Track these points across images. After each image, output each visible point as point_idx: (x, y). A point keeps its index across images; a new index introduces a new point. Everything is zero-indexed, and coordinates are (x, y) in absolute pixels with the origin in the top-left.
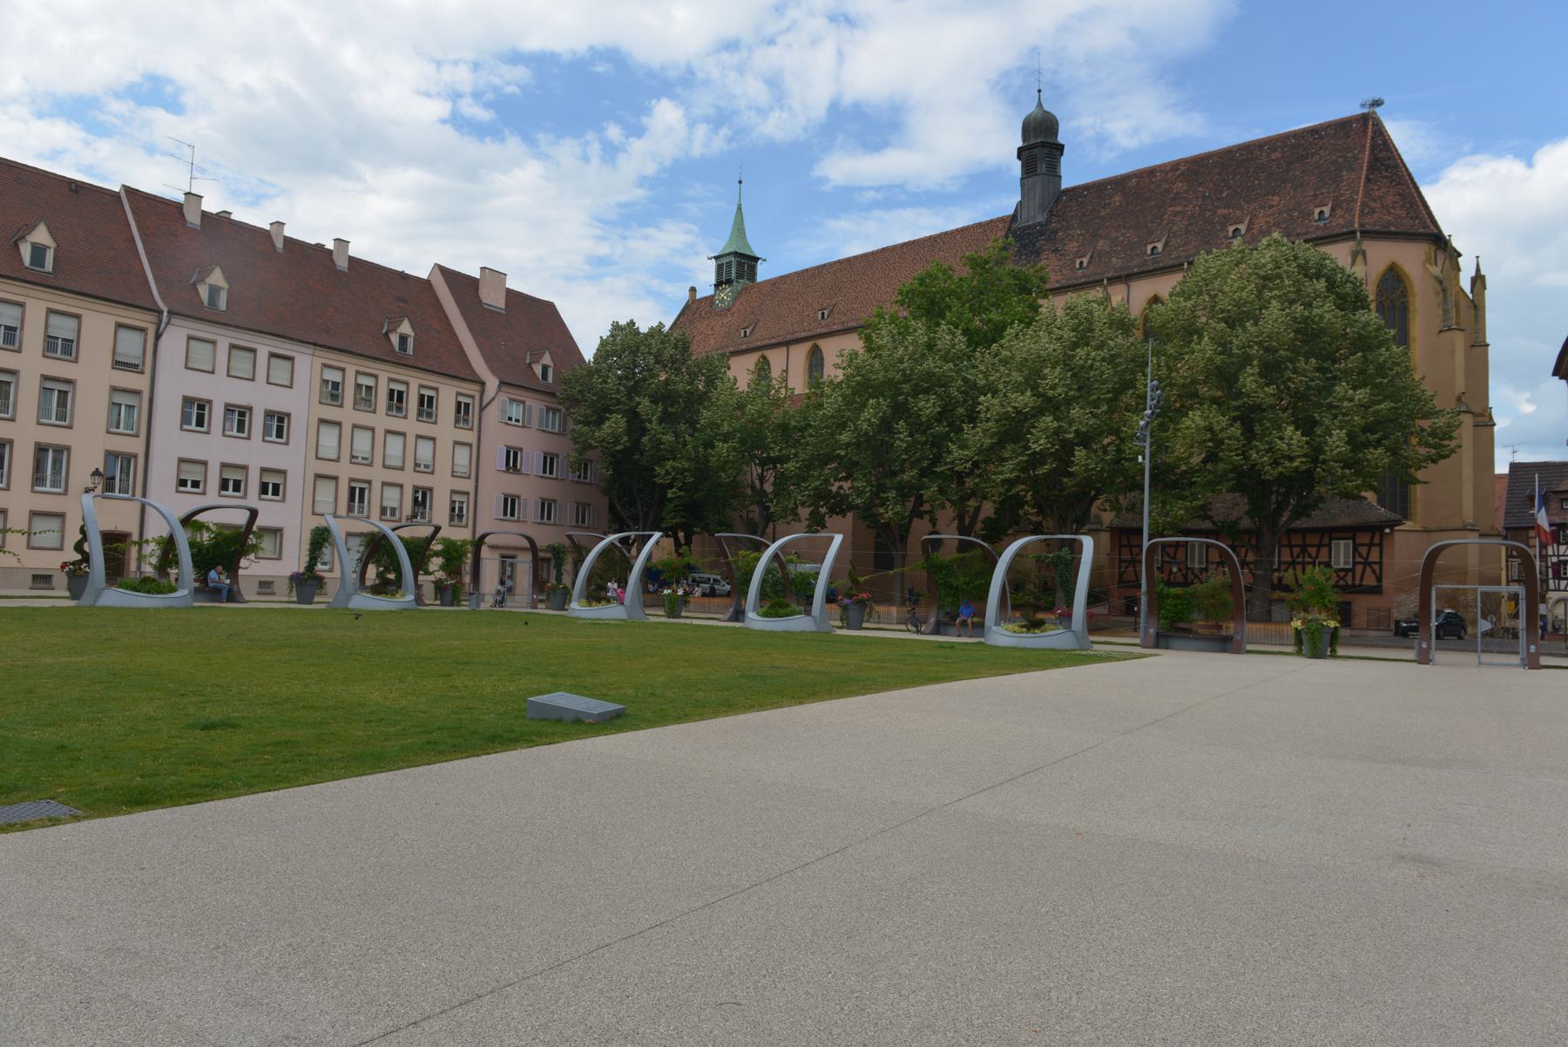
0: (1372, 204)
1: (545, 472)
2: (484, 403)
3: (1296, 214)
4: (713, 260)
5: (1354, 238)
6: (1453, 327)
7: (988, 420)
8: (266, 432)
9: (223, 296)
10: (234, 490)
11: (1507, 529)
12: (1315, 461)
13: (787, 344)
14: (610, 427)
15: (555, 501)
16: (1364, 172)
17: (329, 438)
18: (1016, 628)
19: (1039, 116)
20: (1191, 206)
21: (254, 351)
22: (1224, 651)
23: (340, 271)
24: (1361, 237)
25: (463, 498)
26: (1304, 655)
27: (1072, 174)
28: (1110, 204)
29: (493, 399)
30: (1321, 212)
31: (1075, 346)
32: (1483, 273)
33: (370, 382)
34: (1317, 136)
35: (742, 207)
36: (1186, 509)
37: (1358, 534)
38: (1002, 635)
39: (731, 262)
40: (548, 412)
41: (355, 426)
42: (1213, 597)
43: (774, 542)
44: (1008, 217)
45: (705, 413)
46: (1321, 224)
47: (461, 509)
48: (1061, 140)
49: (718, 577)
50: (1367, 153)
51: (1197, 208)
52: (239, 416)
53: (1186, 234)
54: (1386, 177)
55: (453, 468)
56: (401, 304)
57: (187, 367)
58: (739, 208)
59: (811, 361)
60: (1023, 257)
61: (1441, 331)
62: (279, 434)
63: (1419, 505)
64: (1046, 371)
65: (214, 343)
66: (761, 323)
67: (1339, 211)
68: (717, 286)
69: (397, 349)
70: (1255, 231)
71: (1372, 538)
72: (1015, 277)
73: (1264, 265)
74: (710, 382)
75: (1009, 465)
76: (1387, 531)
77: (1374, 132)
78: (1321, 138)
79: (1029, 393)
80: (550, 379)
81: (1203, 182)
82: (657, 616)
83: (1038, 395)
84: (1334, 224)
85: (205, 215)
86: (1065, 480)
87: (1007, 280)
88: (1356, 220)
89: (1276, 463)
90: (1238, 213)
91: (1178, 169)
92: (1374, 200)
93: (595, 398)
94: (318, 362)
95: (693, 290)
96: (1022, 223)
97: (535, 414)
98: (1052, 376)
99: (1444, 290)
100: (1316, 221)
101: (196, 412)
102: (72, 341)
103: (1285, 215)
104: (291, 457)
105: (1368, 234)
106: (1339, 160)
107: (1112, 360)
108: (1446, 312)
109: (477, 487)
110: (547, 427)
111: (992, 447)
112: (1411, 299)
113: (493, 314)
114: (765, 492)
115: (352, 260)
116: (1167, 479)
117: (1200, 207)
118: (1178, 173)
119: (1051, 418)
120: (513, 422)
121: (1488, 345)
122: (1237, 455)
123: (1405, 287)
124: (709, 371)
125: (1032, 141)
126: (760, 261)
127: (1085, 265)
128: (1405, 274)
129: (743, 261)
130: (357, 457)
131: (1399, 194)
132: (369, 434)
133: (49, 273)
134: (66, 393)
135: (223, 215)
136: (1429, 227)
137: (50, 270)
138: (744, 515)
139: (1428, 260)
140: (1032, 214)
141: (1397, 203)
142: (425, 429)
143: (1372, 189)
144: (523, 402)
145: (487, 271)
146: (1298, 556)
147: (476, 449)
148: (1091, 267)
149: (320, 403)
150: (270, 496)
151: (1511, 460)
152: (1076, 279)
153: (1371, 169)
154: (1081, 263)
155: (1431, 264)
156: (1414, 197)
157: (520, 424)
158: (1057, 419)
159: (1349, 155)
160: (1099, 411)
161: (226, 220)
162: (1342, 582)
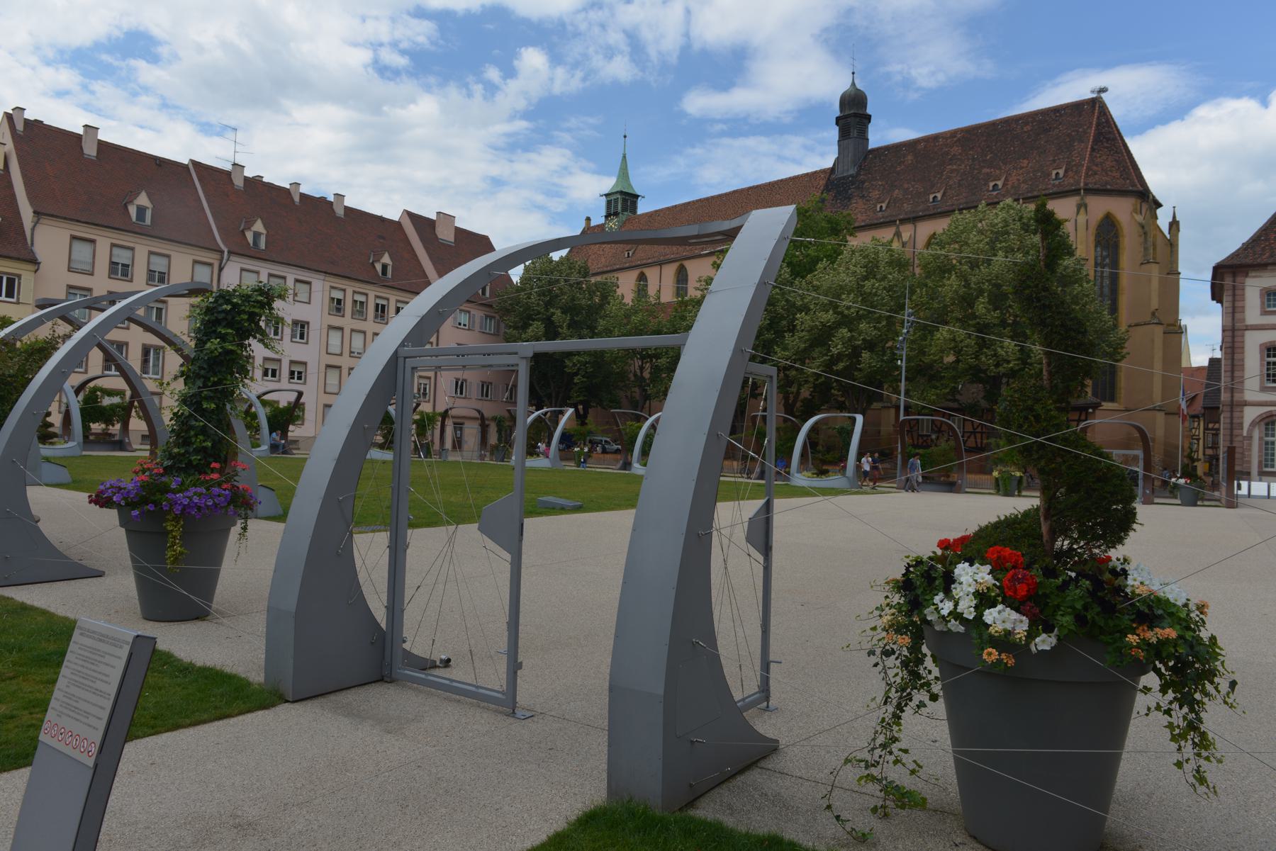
7: (802, 331)
10: (272, 376)
11: (1205, 408)
12: (1025, 363)
13: (660, 264)
14: (533, 331)
15: (491, 383)
17: (335, 339)
18: (810, 474)
19: (853, 93)
22: (951, 491)
25: (426, 381)
26: (1000, 495)
27: (881, 135)
30: (1057, 173)
31: (866, 278)
33: (362, 298)
36: (937, 395)
38: (801, 479)
40: (486, 319)
41: (352, 330)
42: (943, 456)
43: (650, 416)
45: (602, 322)
46: (1057, 182)
47: (425, 389)
48: (869, 111)
49: (608, 439)
54: (1107, 148)
56: (382, 241)
58: (624, 157)
59: (678, 277)
61: (1142, 264)
62: (302, 337)
63: (1123, 391)
64: (844, 296)
68: (606, 217)
70: (1009, 187)
71: (1080, 416)
72: (829, 222)
73: (997, 224)
74: (604, 298)
75: (818, 362)
76: (1090, 410)
77: (1100, 113)
78: (1061, 115)
79: (831, 312)
80: (488, 294)
81: (973, 147)
82: (570, 466)
83: (838, 313)
84: (1066, 183)
85: (246, 179)
86: (856, 373)
87: (824, 224)
89: (997, 365)
90: (998, 172)
92: (1097, 165)
93: (521, 309)
94: (328, 285)
95: (588, 219)
96: (838, 174)
97: (477, 320)
98: (848, 303)
99: (1145, 233)
102: (165, 273)
107: (889, 289)
108: (1146, 249)
110: (486, 329)
111: (805, 350)
113: (445, 246)
114: (644, 378)
115: (347, 208)
116: (923, 372)
117: (970, 166)
118: (955, 139)
119: (846, 330)
120: (462, 326)
121: (1179, 273)
122: (972, 358)
123: (1117, 230)
124: (604, 289)
126: (640, 198)
128: (1118, 221)
130: (354, 353)
131: (1116, 160)
132: (362, 336)
134: (161, 309)
137: (149, 224)
138: (629, 394)
139: (1135, 211)
140: (846, 168)
143: (1096, 157)
144: (469, 312)
149: (329, 314)
150: (270, 378)
151: (1210, 356)
152: (877, 219)
153: (1096, 141)
154: (881, 207)
155: (1136, 213)
157: (467, 327)
158: (850, 331)
159: (1081, 130)
160: (880, 326)
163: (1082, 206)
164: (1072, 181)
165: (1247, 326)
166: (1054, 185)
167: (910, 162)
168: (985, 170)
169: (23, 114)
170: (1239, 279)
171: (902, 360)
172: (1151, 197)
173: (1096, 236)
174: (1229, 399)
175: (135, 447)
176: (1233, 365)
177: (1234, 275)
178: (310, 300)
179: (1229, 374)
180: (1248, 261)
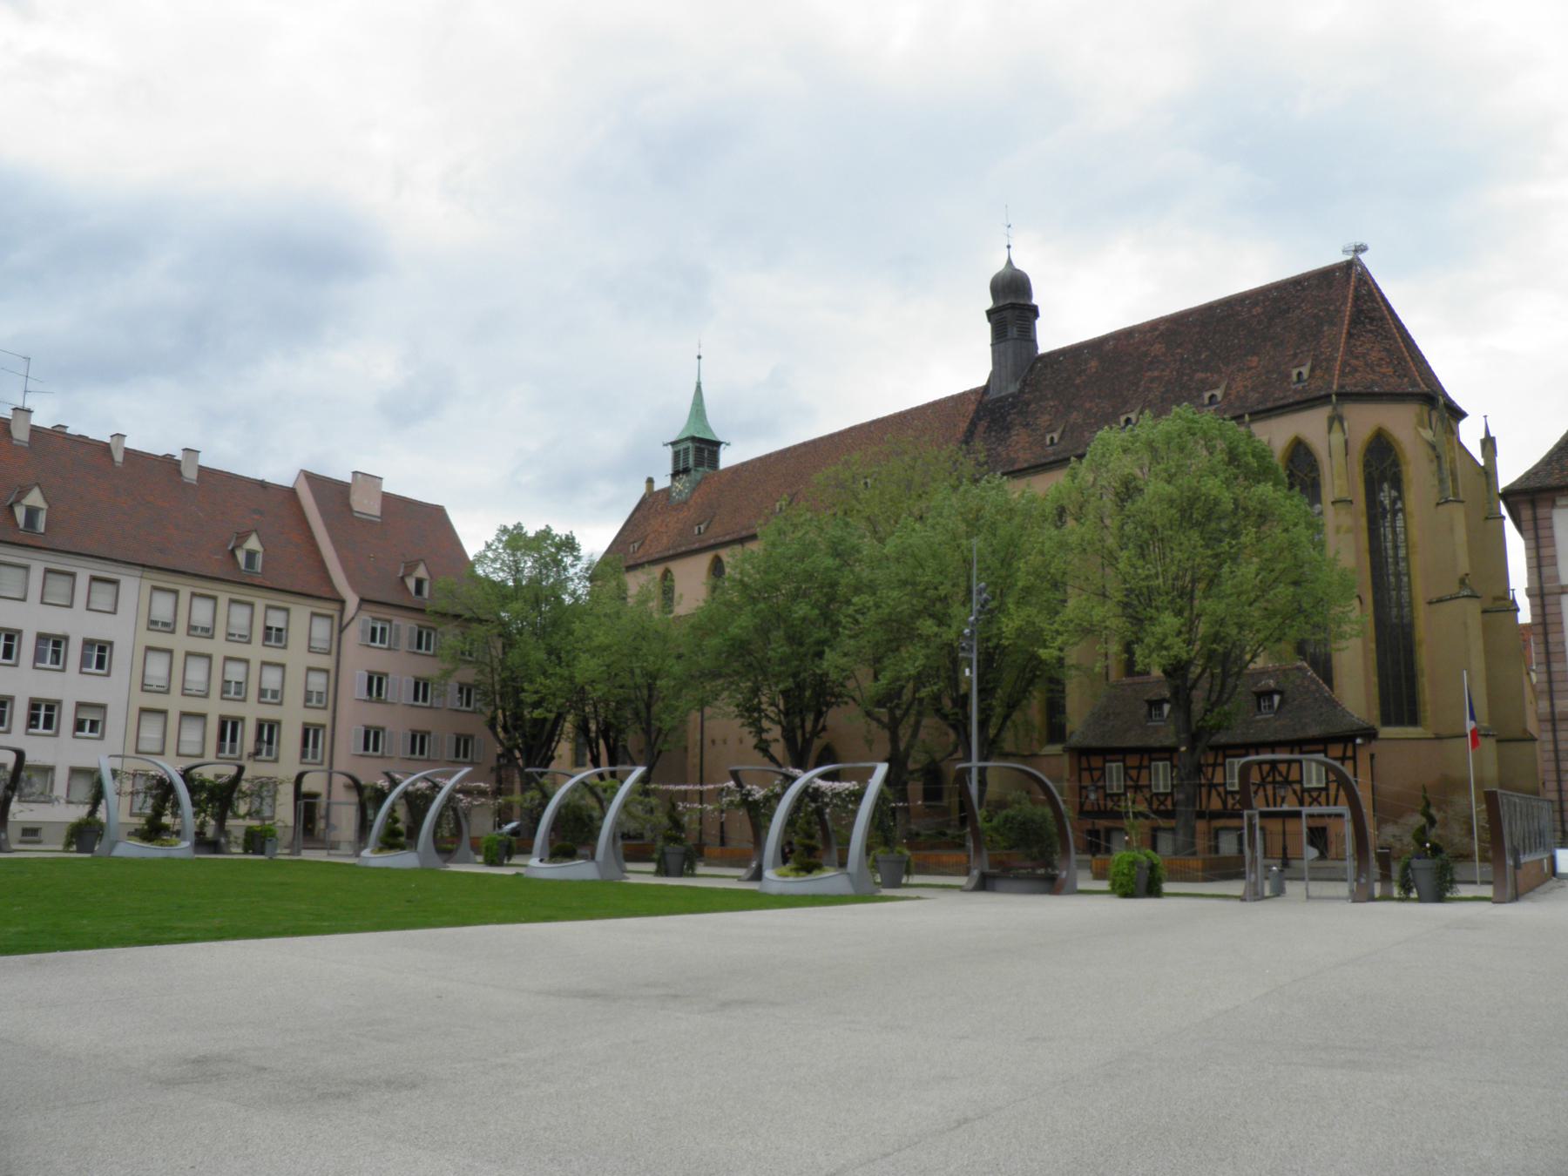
0: (1354, 362)
1: (416, 698)
3: (1275, 376)
4: (670, 447)
5: (1330, 402)
6: (1451, 498)
8: (85, 662)
9: (42, 519)
16: (1346, 327)
17: (157, 668)
20: (1168, 370)
21: (73, 575)
24: (1337, 400)
27: (1051, 336)
28: (1085, 370)
29: (353, 618)
30: (1300, 374)
32: (1492, 435)
34: (1299, 288)
37: (1128, 757)
38: (775, 879)
39: (688, 448)
41: (188, 654)
44: (981, 388)
46: (1300, 386)
48: (1035, 301)
50: (1349, 305)
51: (1175, 373)
52: (52, 646)
53: (1162, 402)
54: (1371, 331)
56: (255, 517)
60: (993, 434)
61: (1438, 504)
62: (100, 665)
63: (1428, 707)
65: (26, 568)
66: (718, 517)
67: (1318, 372)
69: (243, 567)
70: (1232, 397)
78: (1304, 289)
84: (1313, 386)
88: (1336, 381)
90: (1216, 377)
91: (1156, 329)
92: (1357, 358)
94: (147, 585)
95: (650, 481)
96: (993, 395)
99: (1438, 457)
100: (1294, 384)
103: (1264, 377)
105: (1345, 396)
106: (1321, 313)
108: (1441, 481)
109: (334, 719)
112: (1404, 468)
113: (366, 523)
115: (202, 469)
123: (1396, 455)
125: (1001, 303)
126: (723, 446)
127: (1056, 440)
129: (703, 446)
131: (1385, 349)
135: (57, 429)
136: (1419, 386)
139: (1421, 423)
141: (1382, 359)
142: (273, 655)
145: (359, 476)
146: (1268, 775)
147: (334, 675)
148: (1063, 443)
150: (86, 733)
152: (1044, 457)
153: (1354, 322)
155: (1424, 428)
156: (1402, 353)
159: (1332, 308)
162: (1162, 808)
163: (1336, 420)
164: (1320, 383)
165: (1562, 587)
166: (1296, 391)
167: (1093, 370)
168: (1200, 375)
170: (1542, 512)
171: (971, 667)
172: (1441, 400)
173: (1365, 466)
174: (1548, 710)
175: (14, 847)
176: (1548, 653)
177: (1534, 505)
178: (116, 609)
179: (1543, 668)
180: (1553, 481)
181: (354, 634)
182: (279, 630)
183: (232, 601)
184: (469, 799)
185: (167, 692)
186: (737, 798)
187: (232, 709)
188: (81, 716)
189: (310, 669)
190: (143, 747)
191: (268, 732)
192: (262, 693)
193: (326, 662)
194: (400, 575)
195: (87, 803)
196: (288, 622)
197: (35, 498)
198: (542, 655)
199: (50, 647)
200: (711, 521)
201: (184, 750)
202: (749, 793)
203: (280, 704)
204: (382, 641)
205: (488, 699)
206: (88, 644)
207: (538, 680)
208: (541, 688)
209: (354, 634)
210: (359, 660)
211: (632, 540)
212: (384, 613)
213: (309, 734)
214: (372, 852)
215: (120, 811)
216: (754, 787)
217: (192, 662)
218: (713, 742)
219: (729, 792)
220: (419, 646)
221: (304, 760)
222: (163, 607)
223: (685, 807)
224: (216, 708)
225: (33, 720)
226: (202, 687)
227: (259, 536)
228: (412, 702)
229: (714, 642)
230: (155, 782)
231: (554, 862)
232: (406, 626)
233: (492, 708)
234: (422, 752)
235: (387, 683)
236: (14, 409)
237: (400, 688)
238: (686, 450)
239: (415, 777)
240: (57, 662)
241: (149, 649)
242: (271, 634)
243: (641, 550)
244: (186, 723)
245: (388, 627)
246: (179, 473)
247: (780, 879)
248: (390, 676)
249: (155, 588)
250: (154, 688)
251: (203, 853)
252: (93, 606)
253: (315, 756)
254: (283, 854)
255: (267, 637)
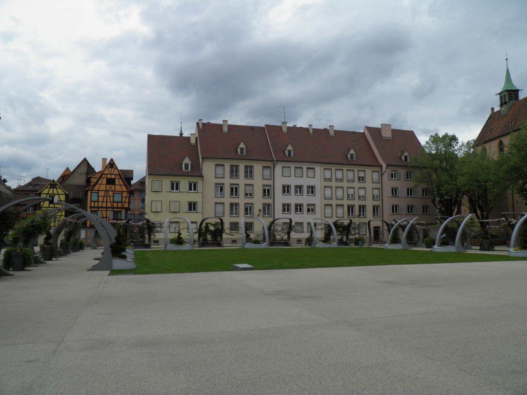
2: (382, 173)
4: (498, 95)
8: (308, 192)
17: (328, 192)
21: (302, 168)
23: (332, 136)
29: (385, 171)
35: (509, 70)
41: (336, 187)
52: (299, 189)
55: (324, 196)
57: (283, 176)
62: (312, 193)
65: (290, 167)
66: (519, 119)
94: (322, 168)
101: (286, 189)
104: (316, 200)
113: (387, 140)
115: (335, 131)
126: (520, 91)
129: (511, 93)
133: (245, 155)
135: (294, 126)
142: (362, 185)
147: (381, 190)
150: (311, 213)
161: (295, 128)
169: (333, 128)
178: (315, 176)
181: (386, 176)
182: (363, 177)
183: (348, 170)
184: (420, 227)
185: (343, 199)
186: (506, 223)
187: (351, 203)
188: (309, 208)
189: (373, 188)
190: (327, 215)
191: (362, 208)
192: (360, 197)
193: (378, 186)
194: (399, 156)
195: (310, 232)
196: (365, 174)
197: (290, 147)
198: (446, 178)
199: (311, 190)
200: (516, 120)
201: (338, 216)
202: (510, 222)
203: (365, 200)
204: (395, 177)
205: (431, 193)
206: (308, 187)
207: (445, 186)
208: (446, 189)
209: (386, 176)
210: (388, 184)
211: (487, 131)
212: (395, 168)
213: (375, 209)
214: (389, 244)
215: (319, 234)
216: (512, 219)
217: (338, 190)
218: (517, 202)
219: (503, 222)
220: (408, 178)
221: (374, 217)
222: (328, 174)
223: (489, 227)
224: (346, 203)
225: (296, 210)
226: (342, 197)
227: (353, 149)
228: (407, 196)
229: (504, 167)
230: (327, 226)
231: (441, 247)
232: (402, 172)
233: (433, 196)
234: (412, 212)
235: (398, 191)
236: (282, 123)
237: (402, 191)
238: (505, 95)
239: (402, 220)
240: (301, 193)
241: (325, 187)
242: (360, 179)
243: (490, 135)
244: (338, 208)
245: (397, 173)
246: (329, 133)
247: (515, 251)
248: (399, 188)
249: (325, 169)
250: (328, 198)
251: (342, 246)
252: (308, 176)
253: (377, 215)
254: (366, 245)
255: (359, 180)
